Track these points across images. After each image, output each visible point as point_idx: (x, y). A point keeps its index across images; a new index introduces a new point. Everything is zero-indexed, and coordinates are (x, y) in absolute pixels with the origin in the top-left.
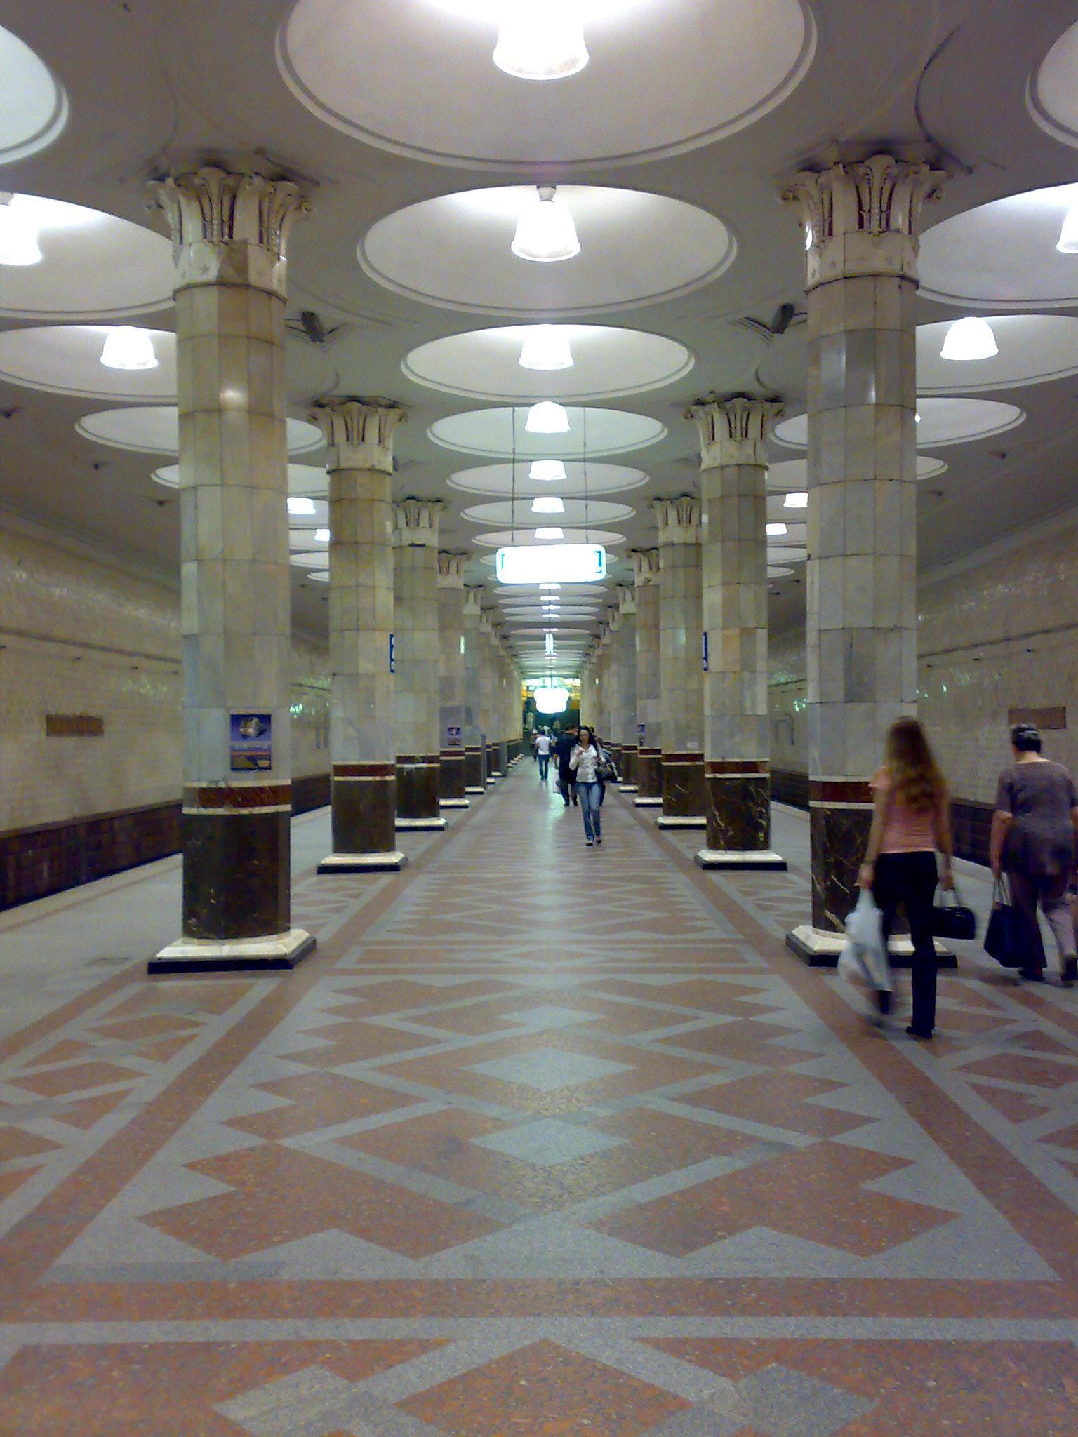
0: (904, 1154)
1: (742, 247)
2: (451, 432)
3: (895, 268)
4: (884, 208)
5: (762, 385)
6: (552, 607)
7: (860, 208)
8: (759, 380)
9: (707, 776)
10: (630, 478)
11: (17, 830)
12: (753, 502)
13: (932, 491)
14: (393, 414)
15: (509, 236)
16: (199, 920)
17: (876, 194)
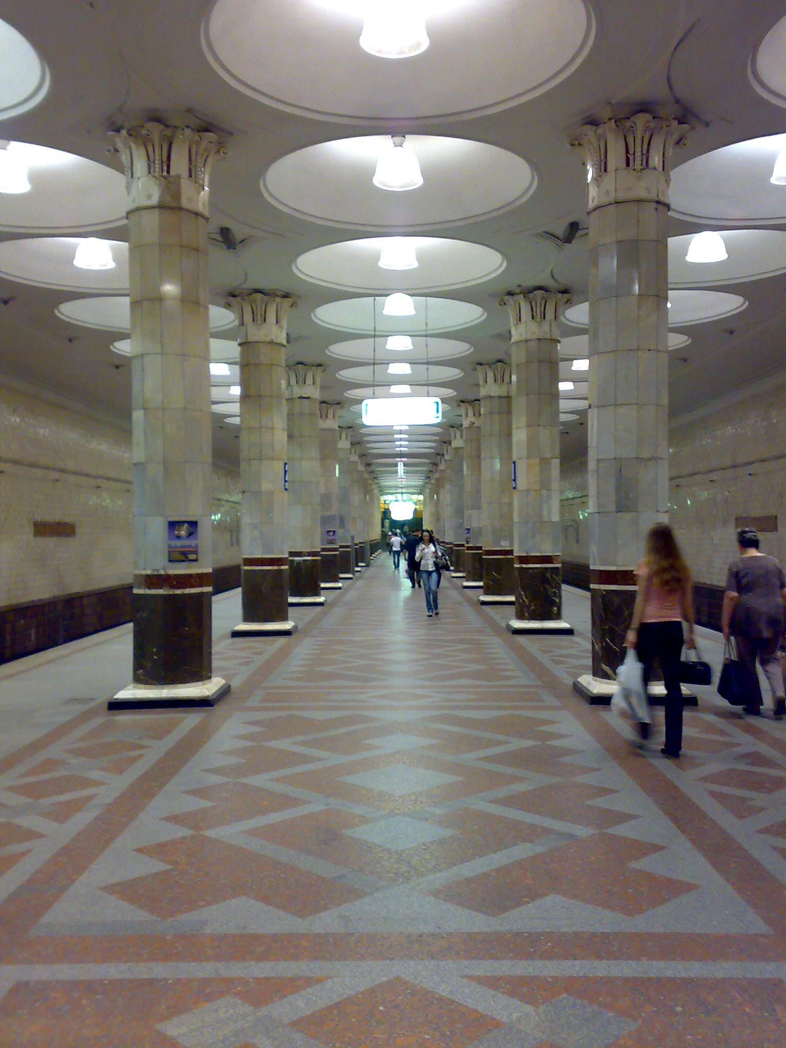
1: (541, 180)
2: (329, 315)
3: (653, 196)
4: (645, 152)
5: (556, 281)
6: (403, 443)
7: (627, 152)
8: (553, 277)
9: (516, 566)
10: (459, 348)
11: (12, 605)
12: (549, 366)
13: (680, 358)
14: (287, 302)
15: (371, 172)
16: (145, 671)
17: (638, 142)
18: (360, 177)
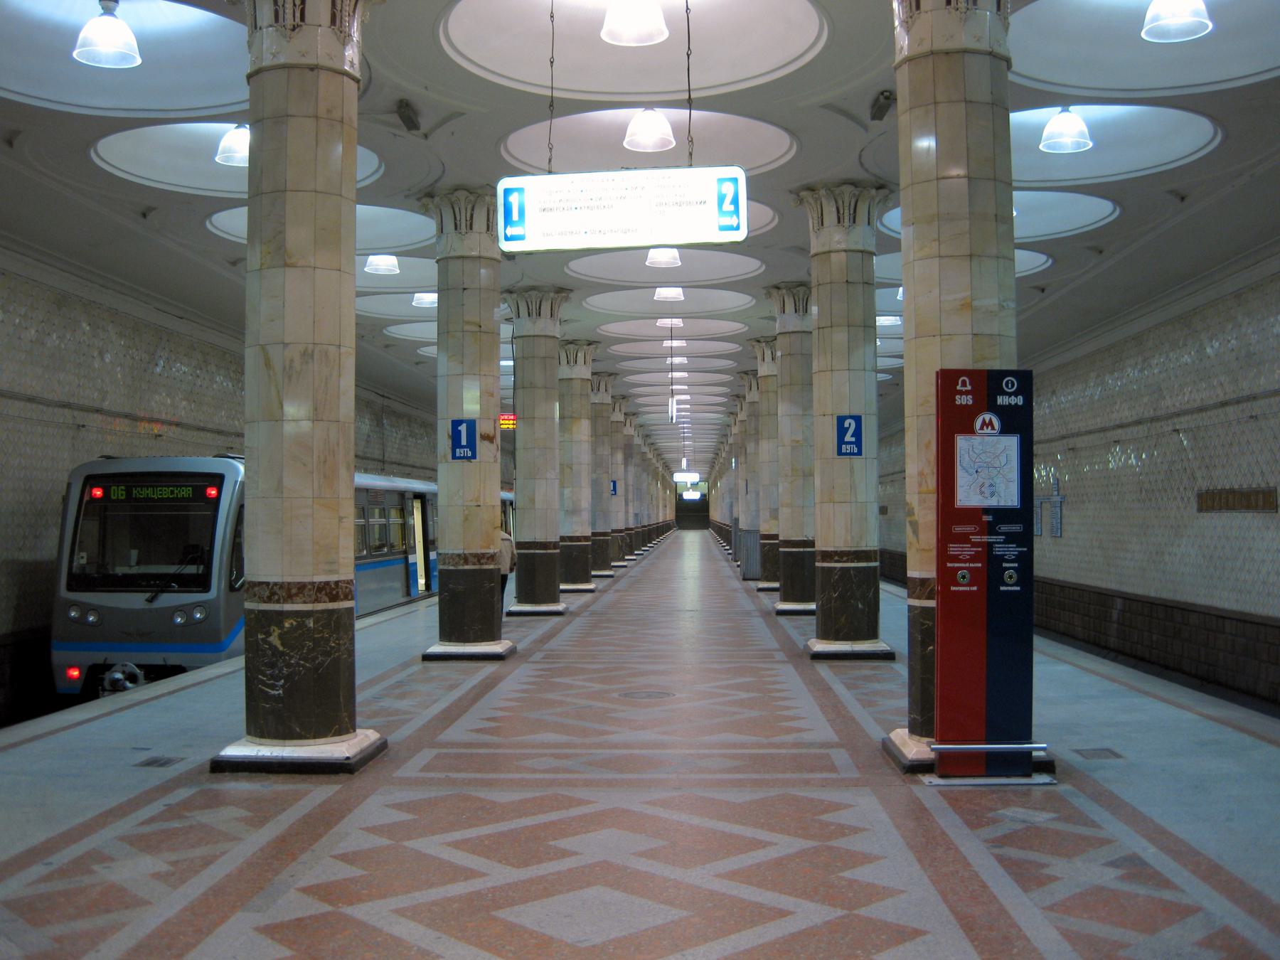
0: (1117, 750)
3: (984, 46)
5: (867, 170)
8: (862, 164)
9: (818, 564)
12: (862, 287)
13: (1035, 286)
15: (599, 24)
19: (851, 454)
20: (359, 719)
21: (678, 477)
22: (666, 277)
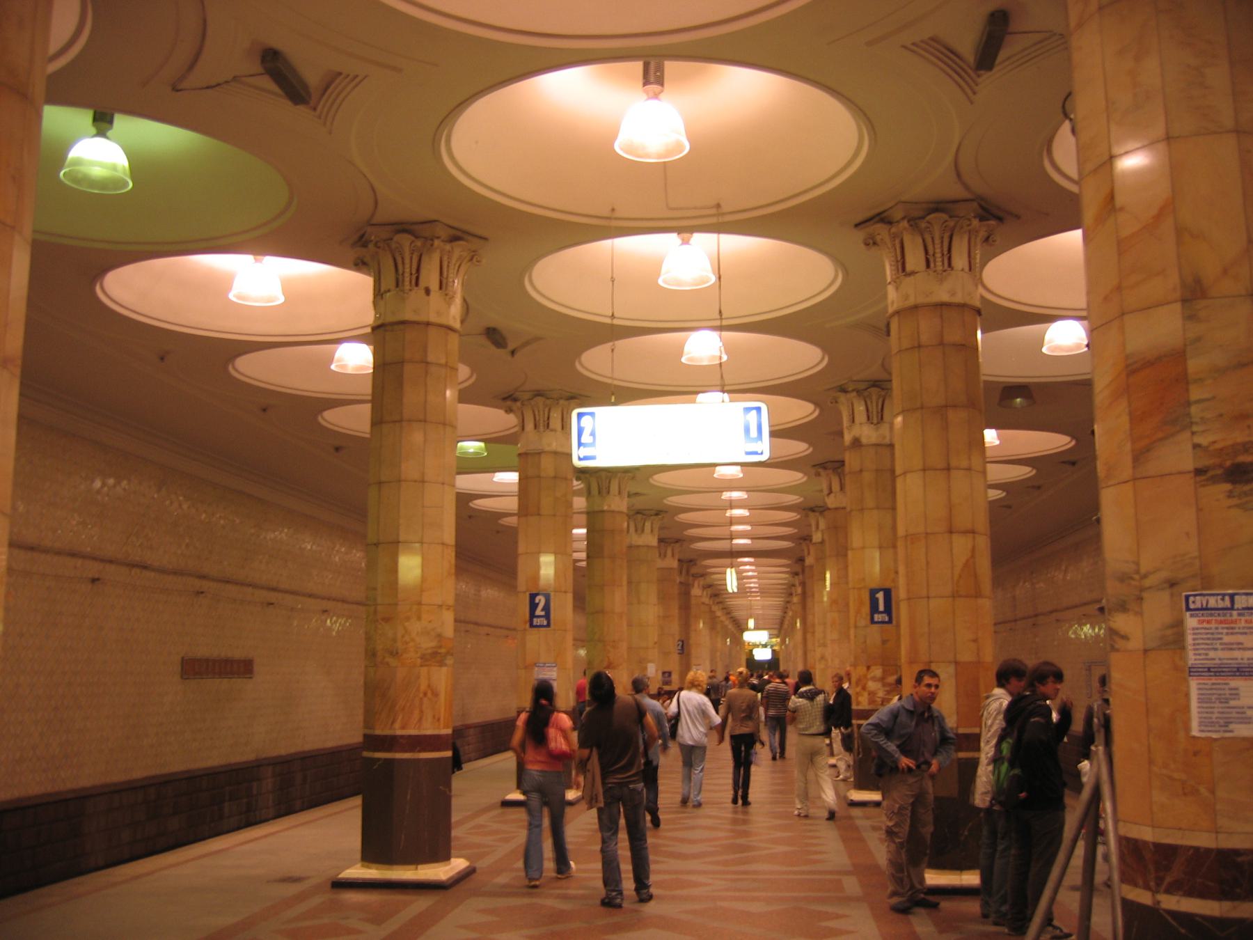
1: (846, 273)
11: (230, 765)
14: (458, 250)
15: (658, 273)
16: (373, 851)
17: (937, 241)
18: (593, 152)
19: (883, 622)
20: (453, 852)
21: (749, 637)
22: (731, 485)
